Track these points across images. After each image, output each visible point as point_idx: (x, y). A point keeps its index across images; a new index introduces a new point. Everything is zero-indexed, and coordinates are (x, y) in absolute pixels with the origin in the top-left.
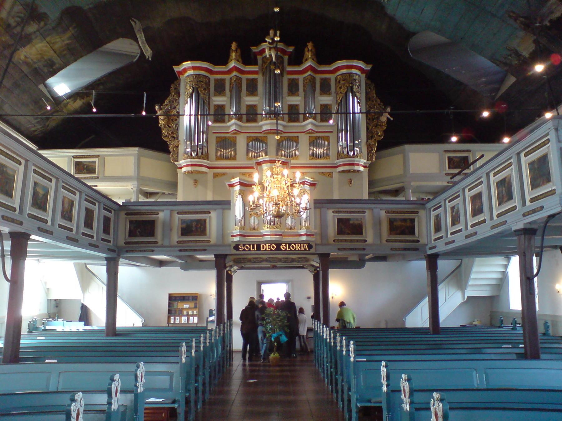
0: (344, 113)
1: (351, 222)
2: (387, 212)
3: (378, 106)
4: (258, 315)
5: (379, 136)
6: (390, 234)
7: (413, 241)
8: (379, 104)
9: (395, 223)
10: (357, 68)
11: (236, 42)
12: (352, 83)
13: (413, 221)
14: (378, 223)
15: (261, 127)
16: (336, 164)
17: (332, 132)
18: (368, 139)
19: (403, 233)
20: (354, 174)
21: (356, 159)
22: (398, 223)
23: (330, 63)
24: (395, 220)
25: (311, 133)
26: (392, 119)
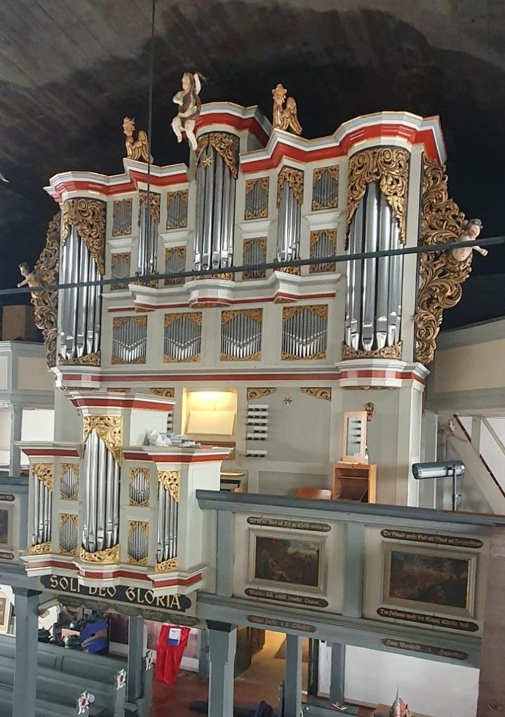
0: (84, 284)
1: (291, 550)
2: (387, 533)
3: (453, 223)
4: (272, 563)
5: (450, 297)
6: (392, 594)
7: (458, 625)
8: (454, 217)
9: (407, 567)
10: (404, 133)
11: (131, 118)
12: (377, 174)
13: (461, 565)
14: (357, 565)
15: (188, 293)
16: (337, 369)
17: (333, 295)
18: (419, 304)
19: (426, 596)
20: (255, 458)
21: (375, 361)
22: (417, 569)
23: (329, 131)
24: (409, 558)
25: (286, 301)
26: (484, 252)
